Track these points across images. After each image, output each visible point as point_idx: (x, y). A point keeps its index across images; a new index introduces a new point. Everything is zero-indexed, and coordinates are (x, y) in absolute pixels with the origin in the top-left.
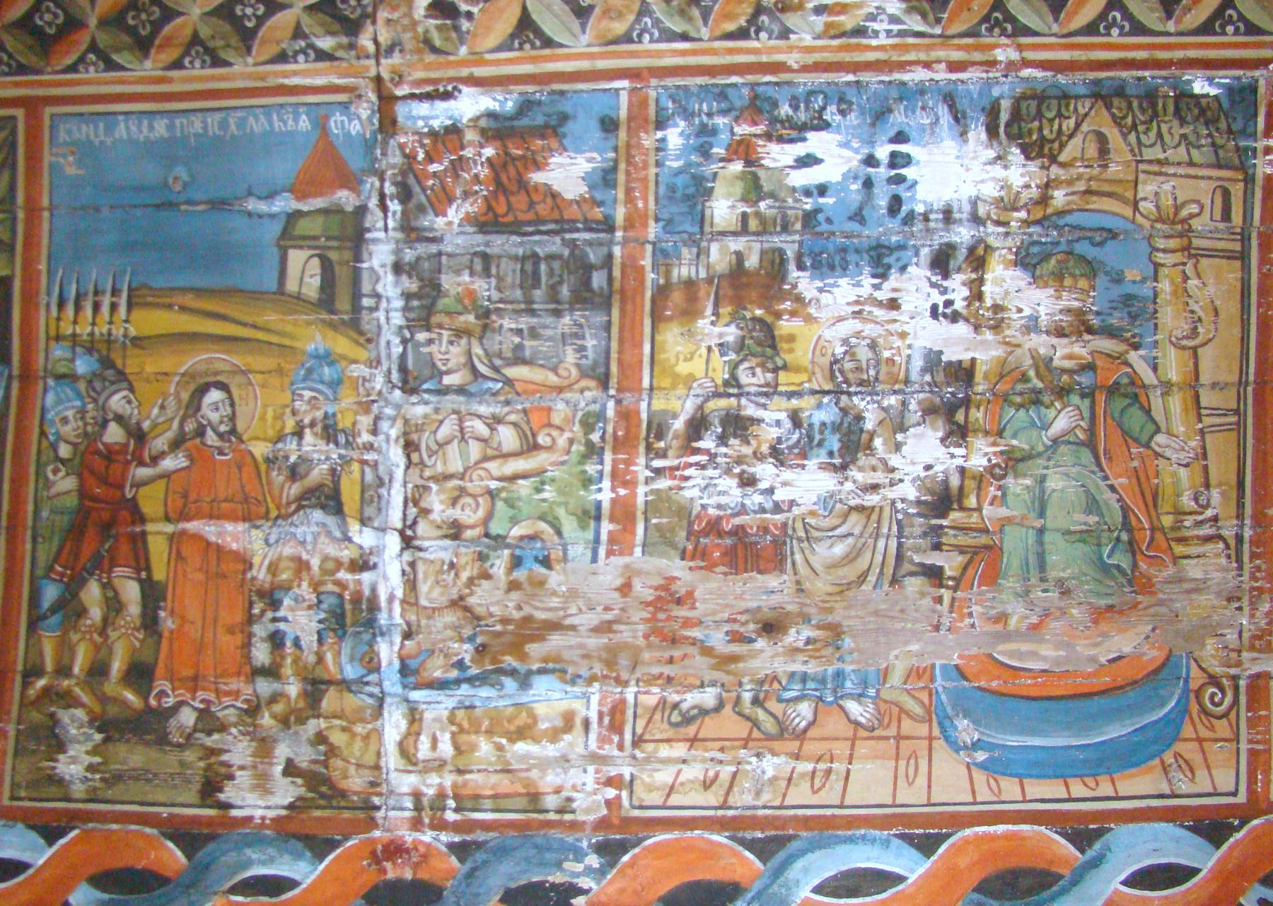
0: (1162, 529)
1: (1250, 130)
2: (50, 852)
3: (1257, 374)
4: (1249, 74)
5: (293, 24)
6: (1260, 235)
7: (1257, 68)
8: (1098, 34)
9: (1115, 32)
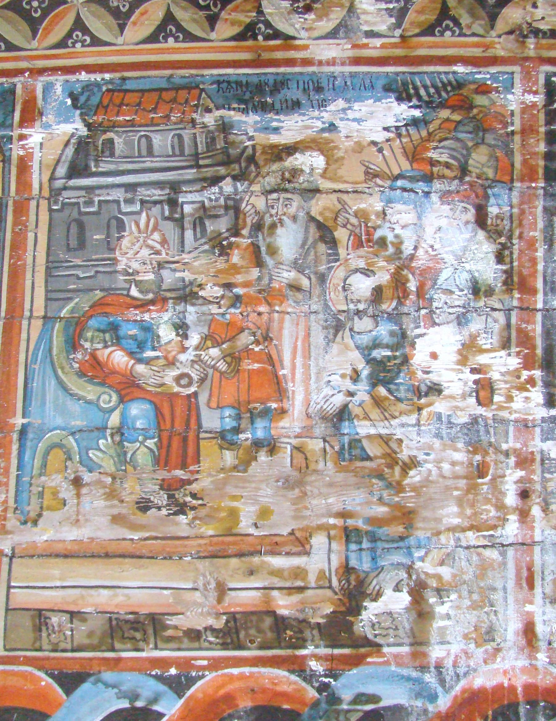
0: (225, 372)
1: (9, 122)
2: (183, 700)
3: (7, 313)
4: (10, 80)
5: (218, 26)
6: (15, 202)
7: (16, 76)
8: (67, 47)
9: (78, 45)
